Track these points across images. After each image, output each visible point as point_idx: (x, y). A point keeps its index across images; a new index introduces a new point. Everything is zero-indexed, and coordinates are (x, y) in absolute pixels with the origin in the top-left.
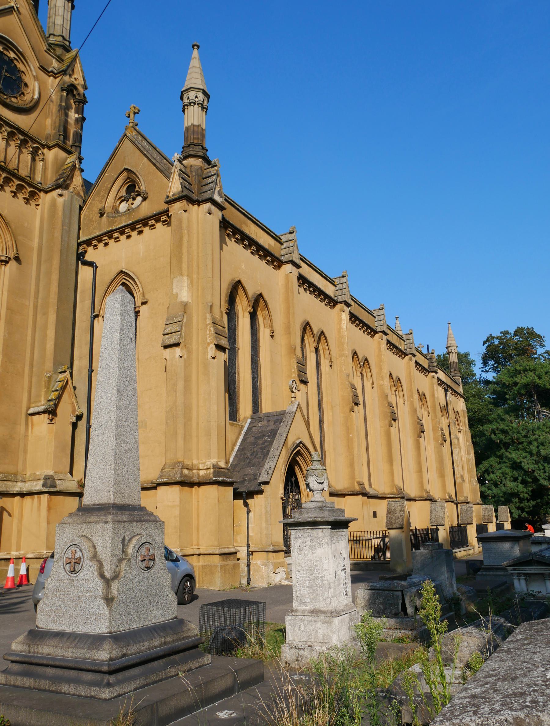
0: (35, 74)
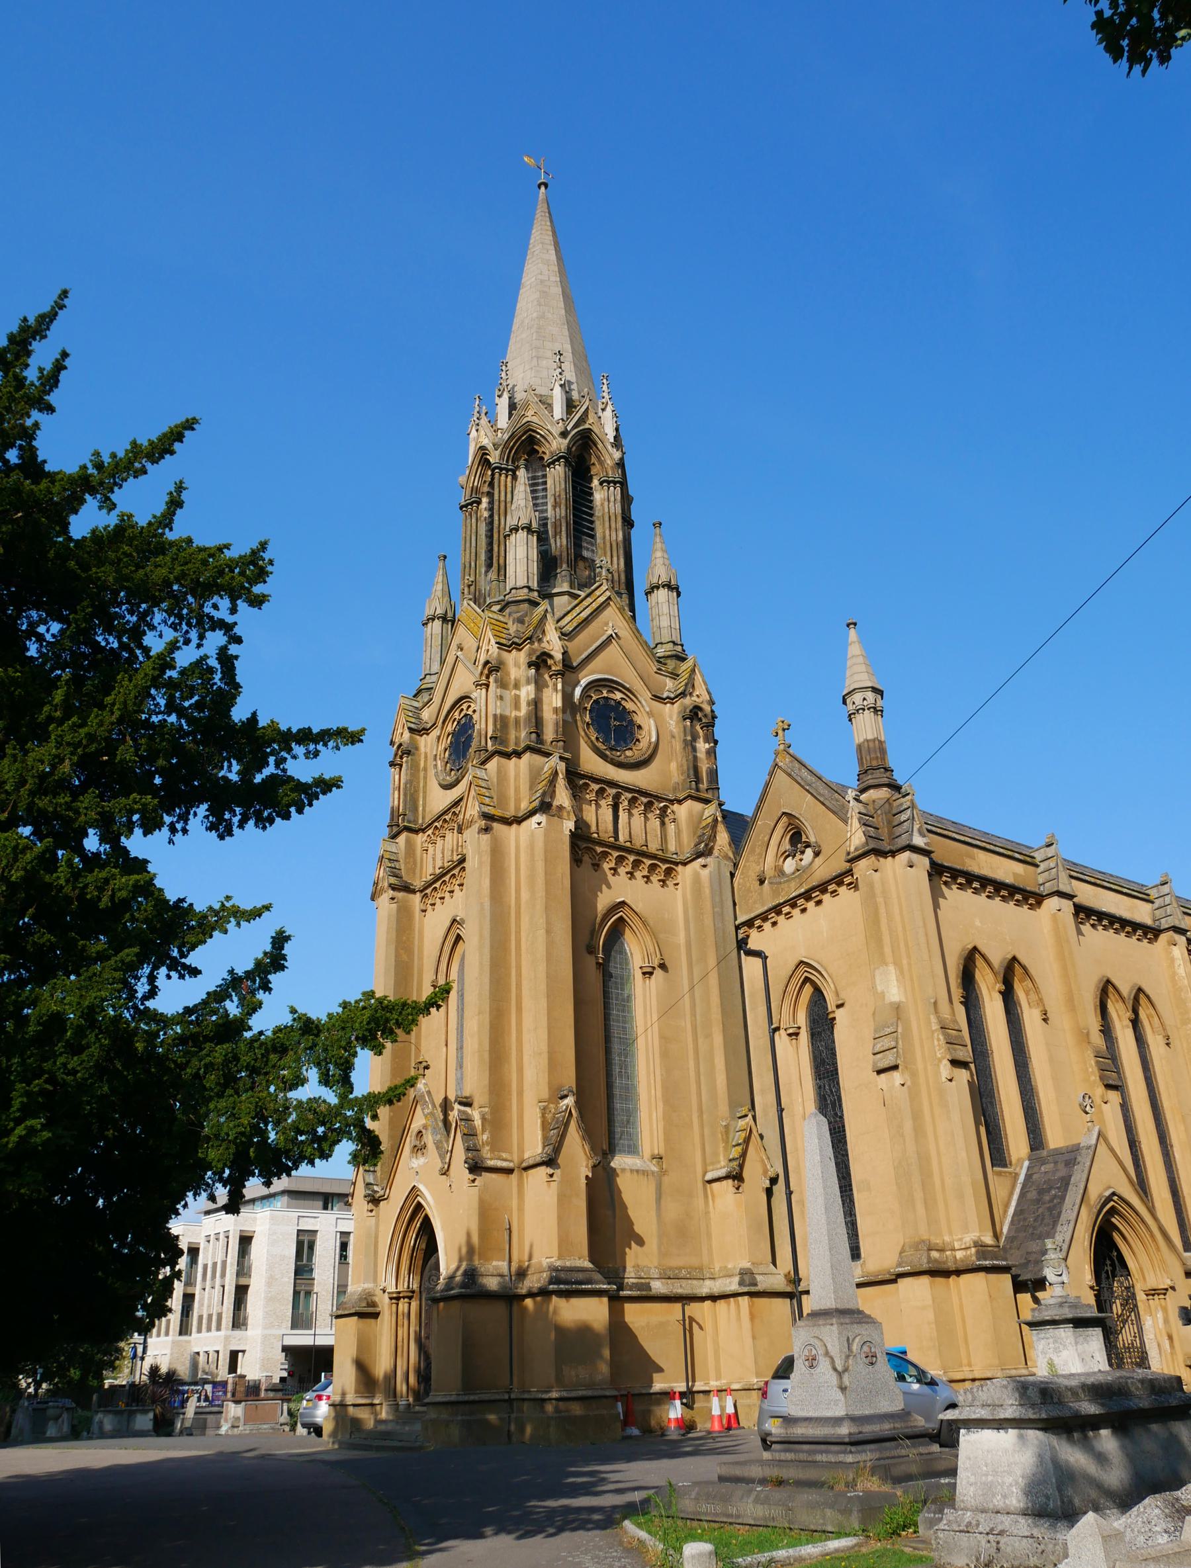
0: (648, 709)
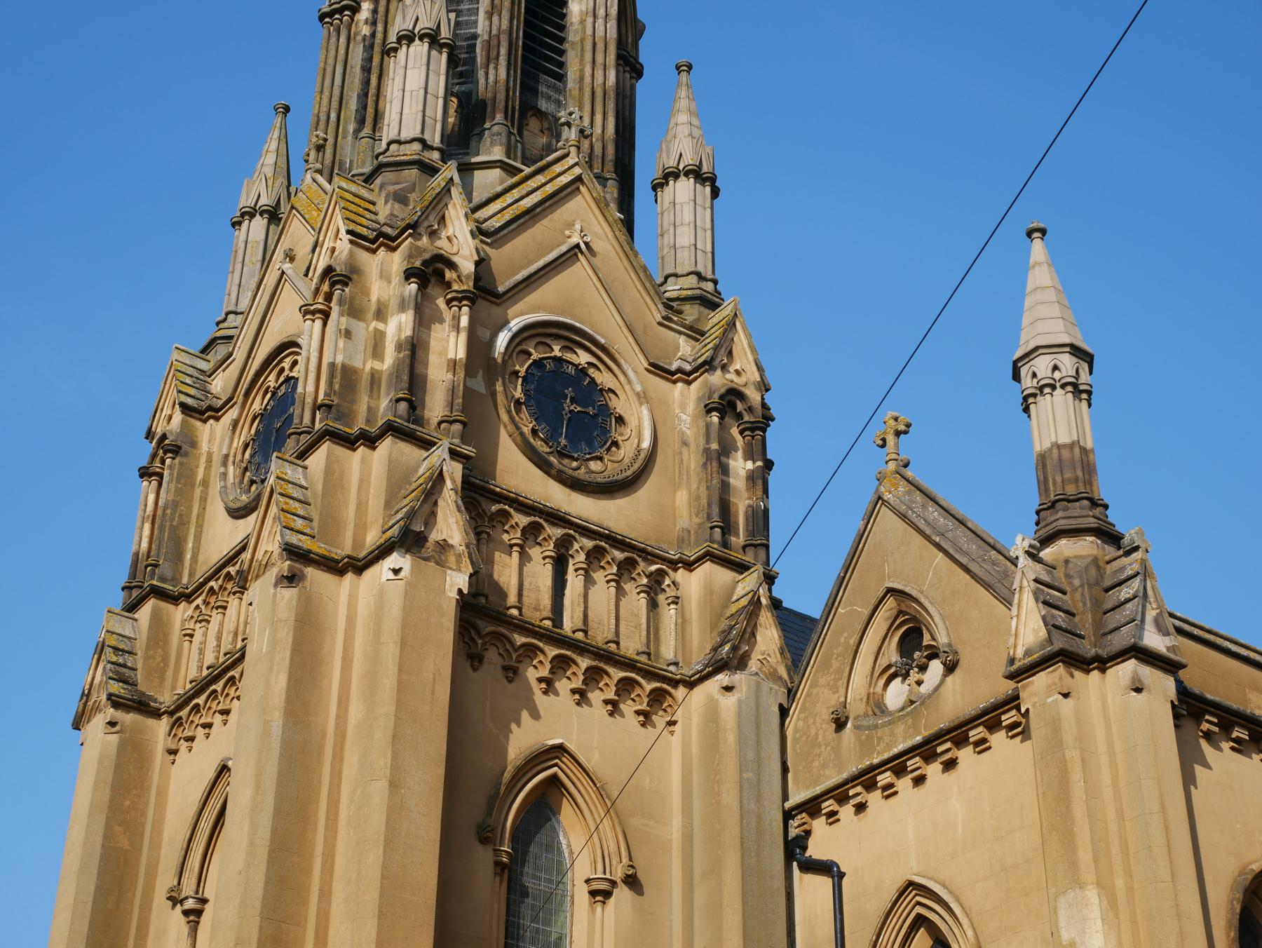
0: (638, 388)
